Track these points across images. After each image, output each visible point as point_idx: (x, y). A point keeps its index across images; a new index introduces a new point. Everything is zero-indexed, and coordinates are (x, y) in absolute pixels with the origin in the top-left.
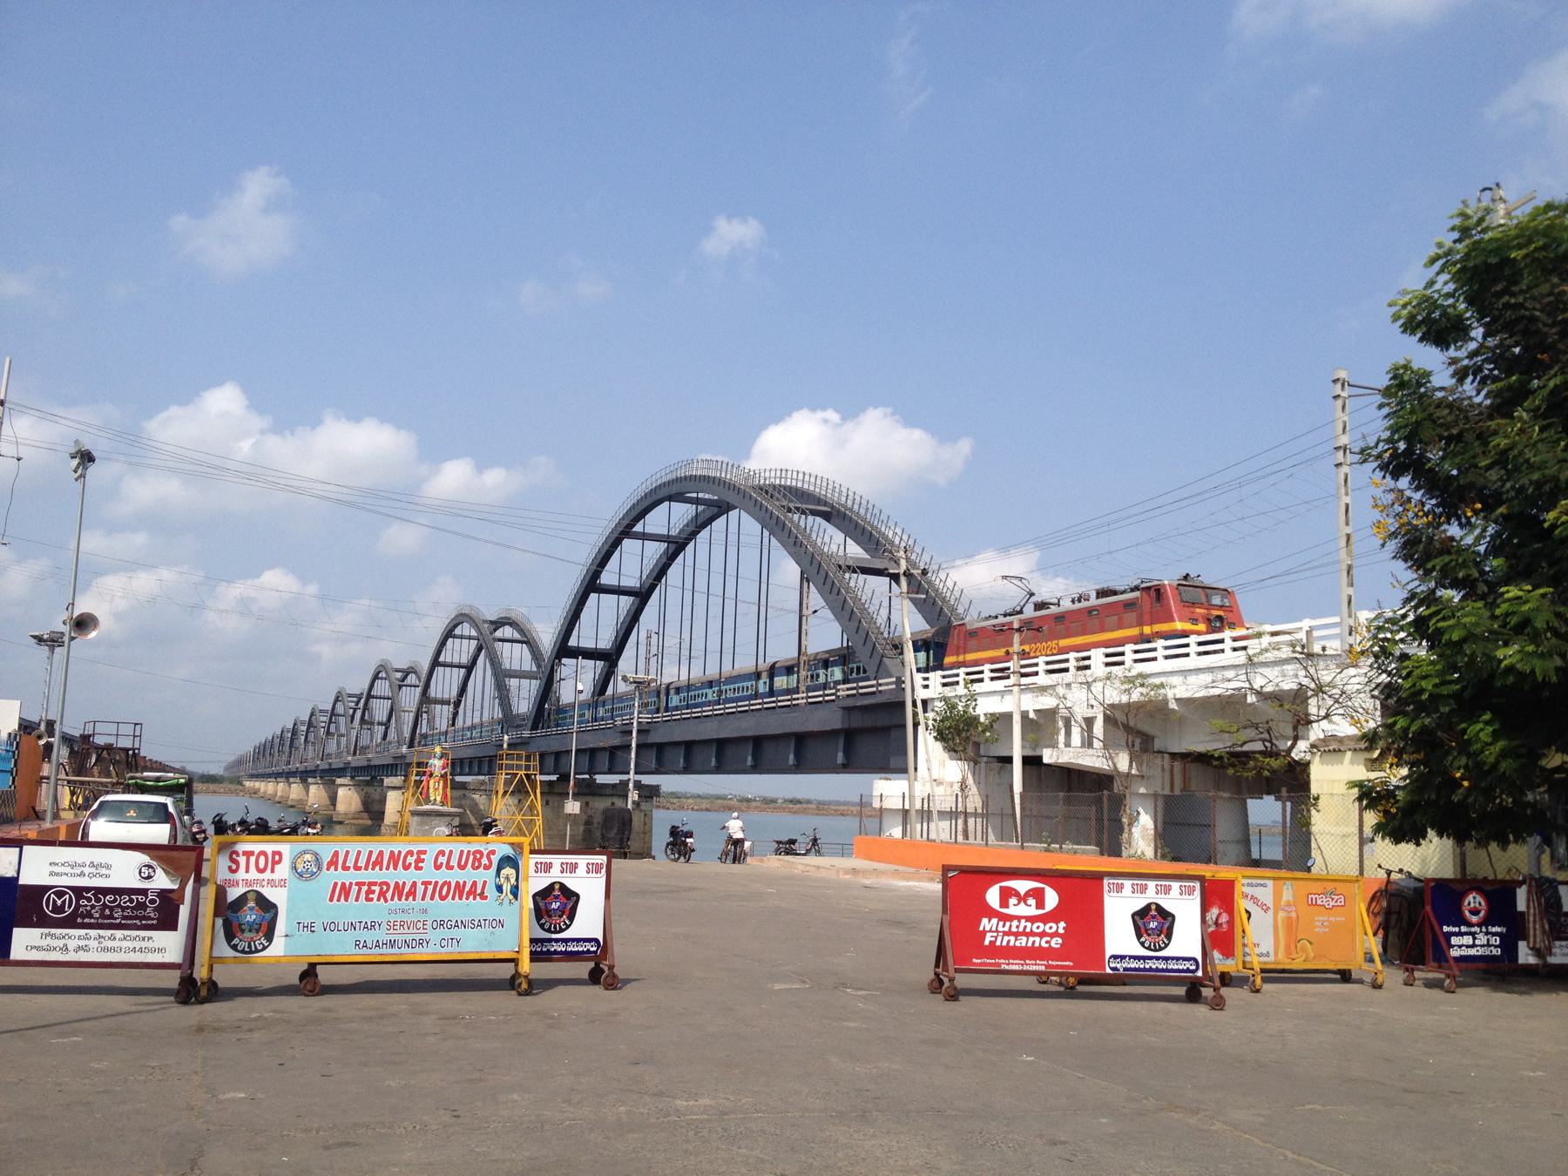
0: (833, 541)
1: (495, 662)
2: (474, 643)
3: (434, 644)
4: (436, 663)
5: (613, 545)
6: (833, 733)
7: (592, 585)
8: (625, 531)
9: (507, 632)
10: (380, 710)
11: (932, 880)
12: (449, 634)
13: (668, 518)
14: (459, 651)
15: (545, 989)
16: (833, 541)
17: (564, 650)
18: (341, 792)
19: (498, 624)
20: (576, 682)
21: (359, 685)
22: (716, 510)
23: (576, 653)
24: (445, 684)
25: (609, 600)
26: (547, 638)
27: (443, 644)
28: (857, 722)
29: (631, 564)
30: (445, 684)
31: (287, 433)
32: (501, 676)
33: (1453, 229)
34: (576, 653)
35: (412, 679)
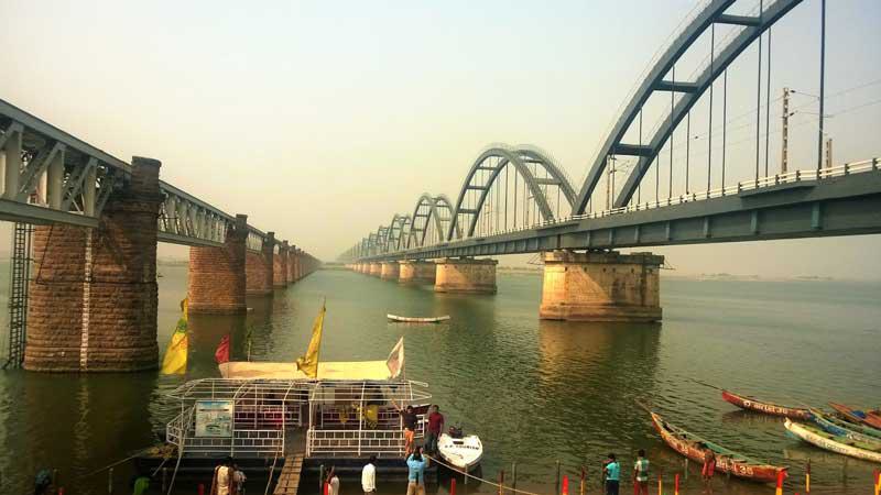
0: (540, 172)
1: (436, 215)
2: (428, 208)
3: (415, 206)
4: (416, 215)
5: (473, 173)
6: (534, 239)
7: (467, 186)
8: (477, 166)
9: (441, 203)
10: (397, 233)
11: (687, 285)
12: (420, 204)
13: (494, 162)
14: (424, 210)
15: (814, 451)
16: (540, 172)
17: (459, 210)
18: (402, 267)
19: (438, 199)
20: (465, 221)
21: (387, 224)
22: (753, 29)
23: (464, 211)
24: (420, 223)
25: (479, 185)
26: (454, 204)
27: (418, 208)
28: (541, 234)
29: (481, 178)
30: (420, 223)
31: (290, 244)
32: (438, 220)
33: (4, 411)
34: (464, 211)
35: (407, 221)
